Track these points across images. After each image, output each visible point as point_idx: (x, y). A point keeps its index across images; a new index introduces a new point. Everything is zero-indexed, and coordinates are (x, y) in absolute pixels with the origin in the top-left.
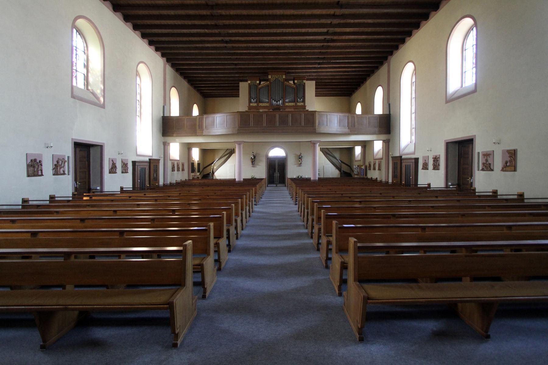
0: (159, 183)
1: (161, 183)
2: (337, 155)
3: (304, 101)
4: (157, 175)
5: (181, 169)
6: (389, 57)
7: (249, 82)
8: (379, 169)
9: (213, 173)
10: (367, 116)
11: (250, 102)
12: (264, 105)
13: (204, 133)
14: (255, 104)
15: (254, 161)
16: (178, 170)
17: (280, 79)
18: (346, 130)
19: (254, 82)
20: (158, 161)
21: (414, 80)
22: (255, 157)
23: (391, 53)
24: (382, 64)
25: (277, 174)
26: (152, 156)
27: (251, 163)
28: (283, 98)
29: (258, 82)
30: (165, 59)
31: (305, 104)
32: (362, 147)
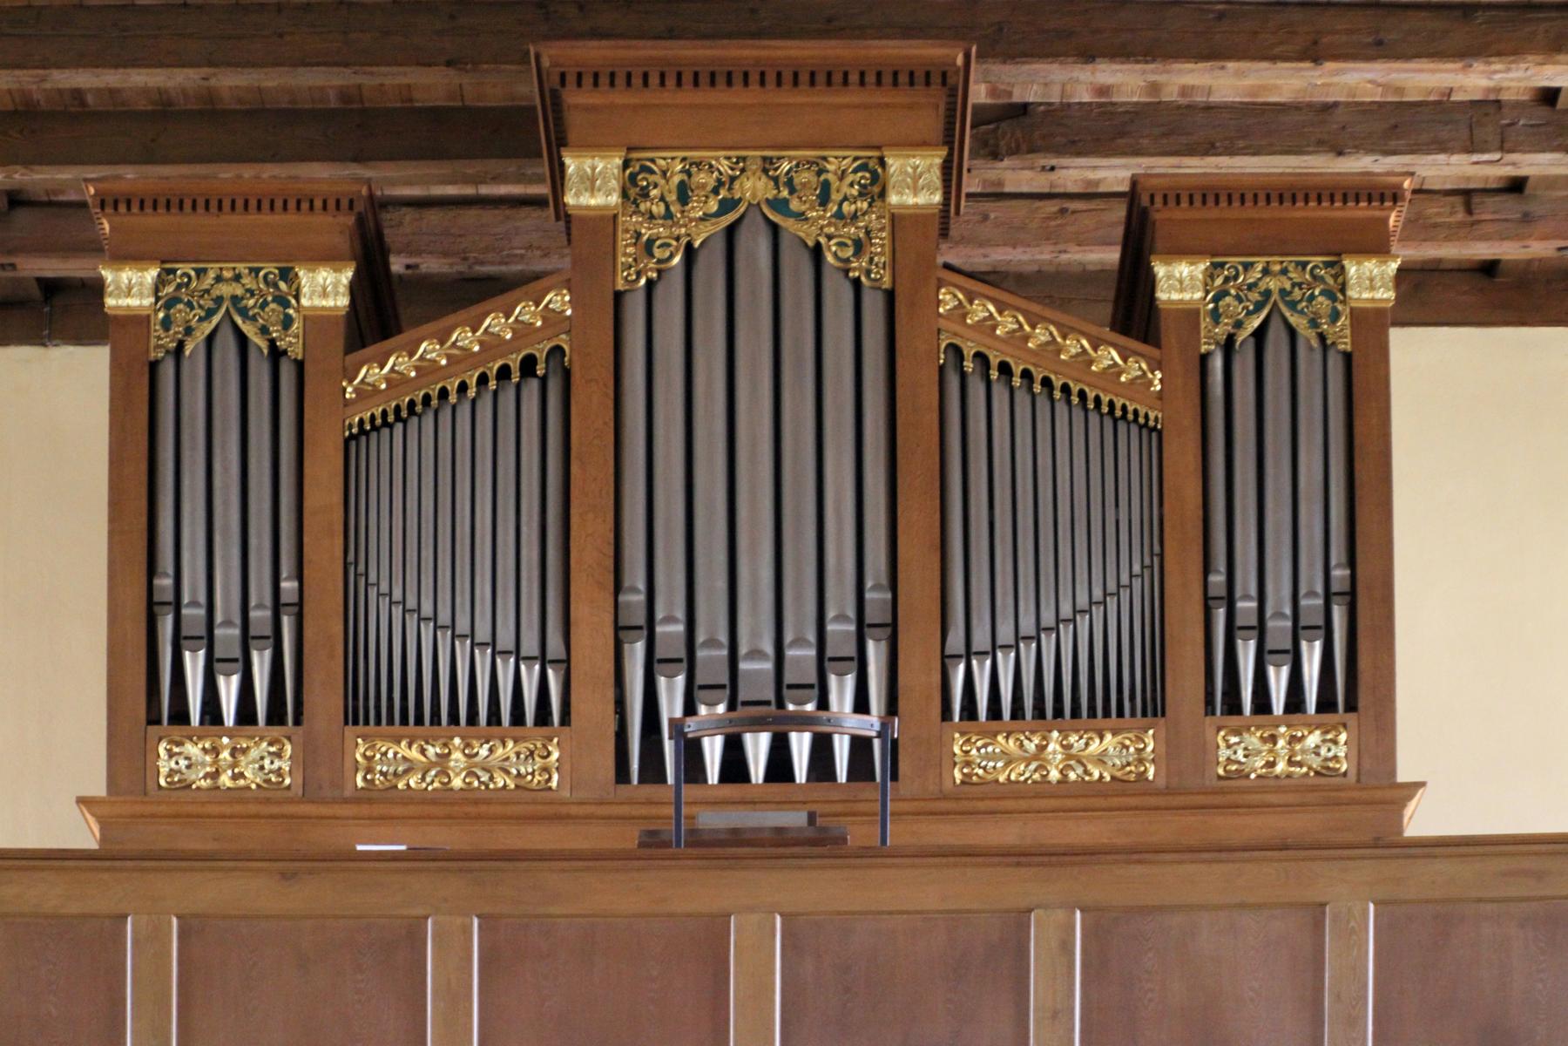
14: (263, 761)
19: (229, 280)
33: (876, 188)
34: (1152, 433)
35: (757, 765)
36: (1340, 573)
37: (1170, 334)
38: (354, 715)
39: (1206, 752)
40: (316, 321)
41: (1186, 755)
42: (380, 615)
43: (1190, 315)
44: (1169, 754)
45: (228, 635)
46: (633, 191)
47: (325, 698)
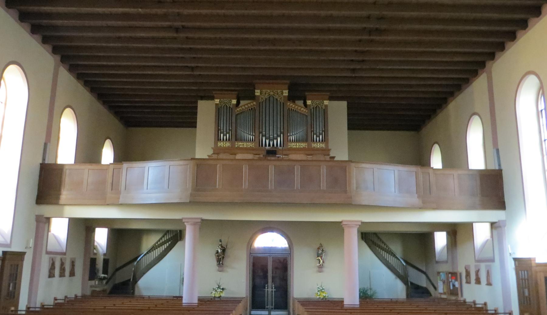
0: (17, 306)
1: (23, 305)
2: (397, 248)
3: (325, 140)
4: (15, 288)
5: (67, 273)
6: (488, 64)
7: (217, 101)
8: (489, 284)
9: (135, 280)
10: (455, 173)
11: (218, 139)
12: (245, 145)
13: (121, 201)
14: (228, 144)
15: (221, 258)
16: (62, 275)
17: (276, 97)
18: (415, 200)
19: (226, 101)
20: (21, 255)
21: (542, 106)
22: (224, 250)
23: (492, 56)
24: (475, 74)
25: (270, 289)
26: (9, 246)
27: (215, 263)
28: (284, 133)
29: (234, 102)
30: (58, 58)
31: (327, 145)
32: (448, 234)
33: (282, 93)
34: (307, 116)
35: (271, 145)
36: (282, 130)
37: (308, 107)
38: (236, 140)
39: (311, 146)
40: (233, 104)
41: (233, 145)
42: (239, 131)
43: (310, 105)
44: (308, 145)
45: (225, 133)
46: (261, 93)
47: (234, 139)
